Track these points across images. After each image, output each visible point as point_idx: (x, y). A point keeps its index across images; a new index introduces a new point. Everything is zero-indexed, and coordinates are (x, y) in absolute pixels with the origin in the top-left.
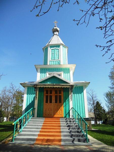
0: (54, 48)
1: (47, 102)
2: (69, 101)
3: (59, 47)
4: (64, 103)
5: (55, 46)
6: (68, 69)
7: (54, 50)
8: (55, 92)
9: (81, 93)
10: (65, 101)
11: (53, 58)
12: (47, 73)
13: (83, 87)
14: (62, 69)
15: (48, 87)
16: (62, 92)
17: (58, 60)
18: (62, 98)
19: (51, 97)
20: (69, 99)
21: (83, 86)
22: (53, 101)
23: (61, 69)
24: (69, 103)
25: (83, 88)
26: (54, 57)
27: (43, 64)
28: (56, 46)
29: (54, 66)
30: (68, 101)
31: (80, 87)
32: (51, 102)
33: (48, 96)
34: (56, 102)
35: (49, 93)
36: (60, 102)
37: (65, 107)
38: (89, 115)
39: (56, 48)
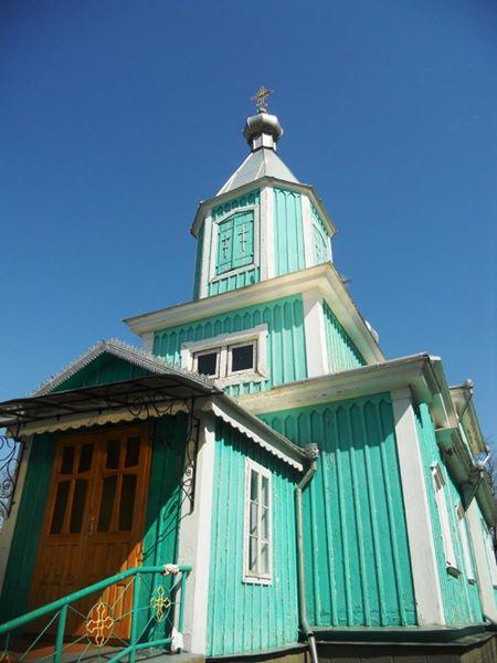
0: (233, 211)
1: (56, 528)
2: (178, 514)
3: (257, 200)
4: (147, 529)
5: (235, 203)
6: (291, 301)
7: (228, 225)
8: (106, 455)
9: (376, 441)
10: (153, 516)
11: (227, 268)
12: (185, 348)
13: (393, 396)
14: (261, 310)
15: (70, 430)
16: (146, 452)
17: (251, 267)
18: (141, 491)
19: (82, 486)
20: (180, 499)
21: (389, 392)
22: (91, 520)
23: (257, 311)
24: (177, 528)
25: (391, 404)
26: (228, 256)
27: (192, 300)
28: (243, 198)
29: (222, 303)
30: (174, 512)
31: (368, 401)
32: (76, 527)
33: (68, 483)
34: (103, 525)
35: (122, 465)
36: (126, 524)
37: (152, 556)
38: (449, 602)
39: (240, 209)
